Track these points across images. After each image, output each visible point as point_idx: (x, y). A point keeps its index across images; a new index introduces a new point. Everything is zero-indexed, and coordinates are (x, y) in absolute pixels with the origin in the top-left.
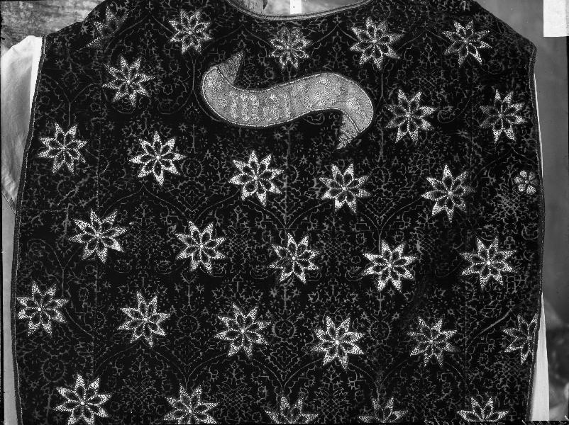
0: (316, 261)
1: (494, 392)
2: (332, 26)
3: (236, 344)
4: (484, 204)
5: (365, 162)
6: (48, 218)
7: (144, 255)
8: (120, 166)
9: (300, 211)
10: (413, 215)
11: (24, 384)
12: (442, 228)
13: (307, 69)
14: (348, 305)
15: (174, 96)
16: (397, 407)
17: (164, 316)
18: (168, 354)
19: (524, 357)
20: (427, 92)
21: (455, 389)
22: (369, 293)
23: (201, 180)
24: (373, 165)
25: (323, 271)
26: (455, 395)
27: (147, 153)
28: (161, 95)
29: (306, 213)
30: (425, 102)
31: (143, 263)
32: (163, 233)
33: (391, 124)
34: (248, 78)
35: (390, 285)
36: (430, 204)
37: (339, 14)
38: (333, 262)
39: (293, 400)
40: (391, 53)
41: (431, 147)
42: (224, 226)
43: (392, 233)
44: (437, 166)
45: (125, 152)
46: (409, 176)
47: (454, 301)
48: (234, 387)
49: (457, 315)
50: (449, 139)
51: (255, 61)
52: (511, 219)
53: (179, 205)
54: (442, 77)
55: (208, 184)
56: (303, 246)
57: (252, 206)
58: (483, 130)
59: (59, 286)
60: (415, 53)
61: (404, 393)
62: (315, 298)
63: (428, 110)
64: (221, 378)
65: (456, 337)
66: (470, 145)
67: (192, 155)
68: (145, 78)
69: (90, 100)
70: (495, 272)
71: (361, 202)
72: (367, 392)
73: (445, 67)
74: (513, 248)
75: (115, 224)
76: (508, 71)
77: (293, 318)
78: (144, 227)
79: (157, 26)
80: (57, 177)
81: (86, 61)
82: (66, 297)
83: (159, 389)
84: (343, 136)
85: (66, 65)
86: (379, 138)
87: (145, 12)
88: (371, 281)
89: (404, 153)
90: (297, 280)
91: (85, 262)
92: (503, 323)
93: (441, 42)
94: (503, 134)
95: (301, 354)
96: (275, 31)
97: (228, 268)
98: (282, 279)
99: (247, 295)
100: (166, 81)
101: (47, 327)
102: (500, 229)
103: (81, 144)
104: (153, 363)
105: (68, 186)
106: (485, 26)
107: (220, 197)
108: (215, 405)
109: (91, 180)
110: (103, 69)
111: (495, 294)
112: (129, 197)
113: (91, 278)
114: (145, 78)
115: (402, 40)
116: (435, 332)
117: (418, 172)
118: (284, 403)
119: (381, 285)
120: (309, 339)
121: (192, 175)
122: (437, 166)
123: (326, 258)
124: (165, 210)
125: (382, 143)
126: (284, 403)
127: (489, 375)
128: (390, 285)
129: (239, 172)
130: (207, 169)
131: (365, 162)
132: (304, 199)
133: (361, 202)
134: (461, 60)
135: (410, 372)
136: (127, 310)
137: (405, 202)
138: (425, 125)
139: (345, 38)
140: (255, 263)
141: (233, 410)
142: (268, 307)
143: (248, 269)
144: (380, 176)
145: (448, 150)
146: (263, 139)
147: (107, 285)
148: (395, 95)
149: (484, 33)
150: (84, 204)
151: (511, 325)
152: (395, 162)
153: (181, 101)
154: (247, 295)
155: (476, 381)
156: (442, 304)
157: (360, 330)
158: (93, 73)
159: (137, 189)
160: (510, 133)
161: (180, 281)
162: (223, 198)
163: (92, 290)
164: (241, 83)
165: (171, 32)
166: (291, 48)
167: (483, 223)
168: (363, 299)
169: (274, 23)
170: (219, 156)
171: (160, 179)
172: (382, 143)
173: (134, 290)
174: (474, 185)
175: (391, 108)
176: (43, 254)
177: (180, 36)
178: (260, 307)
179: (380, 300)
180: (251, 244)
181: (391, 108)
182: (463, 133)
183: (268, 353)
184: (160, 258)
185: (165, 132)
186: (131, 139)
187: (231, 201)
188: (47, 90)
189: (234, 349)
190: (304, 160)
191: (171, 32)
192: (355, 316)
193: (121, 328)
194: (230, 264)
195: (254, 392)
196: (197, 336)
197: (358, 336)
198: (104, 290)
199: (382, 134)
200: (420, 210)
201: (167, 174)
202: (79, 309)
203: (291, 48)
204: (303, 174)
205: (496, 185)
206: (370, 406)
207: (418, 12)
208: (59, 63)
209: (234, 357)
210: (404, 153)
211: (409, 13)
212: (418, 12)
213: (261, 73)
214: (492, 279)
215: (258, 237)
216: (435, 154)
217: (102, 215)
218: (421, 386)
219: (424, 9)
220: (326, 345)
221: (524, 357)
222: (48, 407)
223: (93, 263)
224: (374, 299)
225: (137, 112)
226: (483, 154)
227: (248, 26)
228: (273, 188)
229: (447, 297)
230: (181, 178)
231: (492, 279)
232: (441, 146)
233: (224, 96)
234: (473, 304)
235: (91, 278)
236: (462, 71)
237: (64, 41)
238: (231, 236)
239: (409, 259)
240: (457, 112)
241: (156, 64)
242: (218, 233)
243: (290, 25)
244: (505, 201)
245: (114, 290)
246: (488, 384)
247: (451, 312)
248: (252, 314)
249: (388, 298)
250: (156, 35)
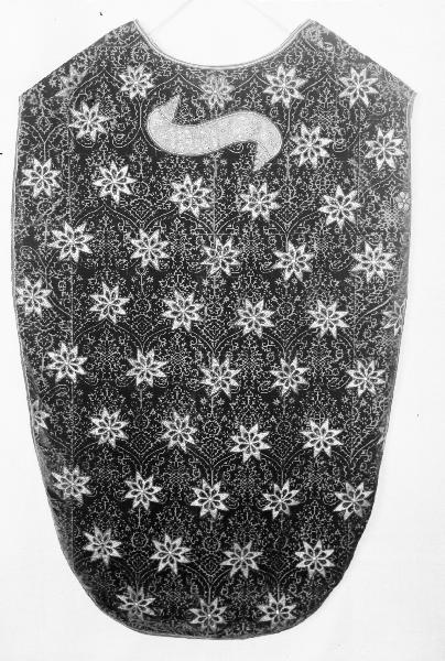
1: (376, 356)
3: (160, 555)
4: (370, 216)
5: (276, 181)
7: (107, 256)
8: (85, 189)
10: (312, 223)
12: (333, 233)
13: (229, 108)
14: (262, 291)
16: (300, 365)
17: (124, 301)
18: (128, 328)
19: (396, 330)
20: (325, 127)
21: (346, 355)
22: (278, 282)
23: (149, 198)
24: (281, 183)
25: (244, 266)
26: (346, 359)
28: (116, 132)
29: (232, 221)
30: (323, 135)
31: (107, 261)
32: (121, 238)
35: (294, 276)
37: (256, 65)
38: (251, 259)
39: (222, 360)
40: (297, 95)
41: (327, 171)
42: (167, 233)
43: (296, 236)
44: (331, 187)
45: (89, 178)
47: (345, 289)
50: (342, 162)
51: (189, 103)
52: (392, 230)
53: (131, 217)
55: (154, 201)
56: (228, 247)
57: (188, 217)
58: (368, 160)
62: (237, 286)
63: (325, 142)
64: (168, 345)
66: (357, 171)
67: (140, 179)
68: (102, 119)
69: (60, 137)
71: (273, 213)
72: (276, 353)
73: (339, 106)
74: (393, 251)
75: (85, 232)
76: (388, 114)
78: (106, 235)
79: (111, 79)
80: (37, 200)
81: (56, 107)
82: (49, 288)
83: (122, 353)
84: (256, 161)
85: (39, 111)
87: (100, 69)
88: (279, 273)
90: (224, 274)
91: (62, 262)
92: (383, 308)
93: (337, 87)
96: (204, 78)
97: (171, 264)
98: (212, 272)
99: (185, 284)
100: (119, 120)
101: (39, 310)
102: (384, 237)
103: (55, 173)
104: (116, 335)
105: (46, 207)
106: (376, 74)
107: (161, 212)
108: (165, 363)
110: (70, 113)
112: (93, 212)
115: (306, 85)
117: (317, 191)
119: (287, 276)
120: (233, 316)
121: (141, 195)
122: (331, 187)
123: (245, 256)
125: (288, 166)
126: (215, 363)
127: (372, 345)
128: (294, 276)
129: (177, 192)
130: (152, 190)
131: (276, 181)
132: (228, 211)
133: (273, 213)
135: (309, 339)
136: (95, 297)
137: (305, 213)
138: (324, 153)
139: (260, 83)
141: (177, 367)
143: (185, 265)
144: (287, 191)
145: (341, 175)
146: (197, 166)
148: (299, 129)
149: (374, 80)
150: (58, 218)
151: (390, 309)
154: (185, 284)
155: (362, 350)
158: (60, 116)
160: (391, 162)
161: (134, 274)
163: (68, 283)
164: (178, 120)
165: (121, 83)
166: (217, 92)
168: (273, 286)
170: (160, 180)
171: (116, 197)
172: (288, 166)
174: (361, 201)
175: (296, 139)
176: (31, 254)
177: (129, 86)
178: (196, 293)
180: (188, 246)
181: (296, 139)
182: (351, 161)
183: (202, 327)
185: (119, 162)
186: (94, 168)
188: (27, 134)
189: (176, 325)
190: (228, 181)
191: (121, 83)
194: (171, 261)
196: (150, 314)
198: (77, 283)
199: (288, 160)
200: (317, 220)
201: (122, 194)
202: (60, 297)
203: (217, 92)
204: (227, 192)
206: (279, 364)
207: (324, 58)
208: (34, 111)
211: (316, 58)
213: (194, 112)
214: (376, 275)
216: (330, 177)
217: (74, 226)
219: (330, 55)
220: (245, 320)
223: (68, 262)
224: (281, 286)
225: (97, 145)
226: (369, 177)
227: (184, 73)
229: (340, 287)
230: (133, 197)
232: (335, 171)
233: (164, 129)
235: (68, 274)
236: (352, 111)
238: (172, 240)
239: (308, 257)
240: (348, 145)
241: (111, 108)
242: (162, 238)
243: (217, 73)
244: (387, 214)
245: (85, 283)
246: (371, 351)
247: (344, 298)
249: (292, 285)
250: (110, 86)
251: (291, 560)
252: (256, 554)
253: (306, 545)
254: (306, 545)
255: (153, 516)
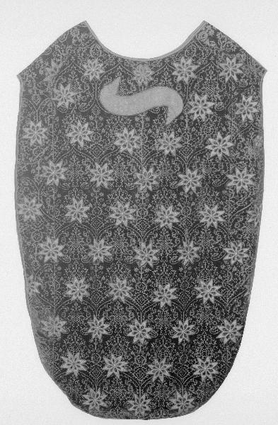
0: (157, 180)
2: (164, 63)
6: (29, 167)
8: (62, 139)
9: (148, 156)
10: (201, 156)
11: (24, 243)
14: (171, 200)
15: (87, 102)
19: (256, 224)
22: (181, 194)
24: (183, 132)
26: (223, 241)
27: (75, 131)
28: (81, 102)
30: (209, 100)
31: (75, 184)
32: (84, 169)
33: (192, 111)
34: (122, 90)
36: (209, 151)
39: (147, 244)
44: (214, 133)
46: (200, 137)
48: (119, 239)
49: (225, 204)
51: (126, 82)
54: (217, 88)
58: (237, 115)
59: (37, 198)
60: (204, 75)
61: (198, 239)
65: (224, 214)
67: (96, 131)
68: (72, 94)
70: (244, 184)
76: (249, 86)
77: (146, 207)
79: (77, 68)
80: (33, 147)
81: (44, 88)
86: (185, 118)
89: (198, 125)
92: (248, 209)
94: (247, 117)
95: (150, 223)
96: (135, 67)
97: (115, 184)
98: (141, 189)
100: (83, 94)
104: (82, 230)
105: (38, 151)
109: (50, 147)
111: (244, 195)
113: (52, 193)
114: (72, 94)
116: (213, 212)
117: (205, 136)
118: (143, 245)
122: (214, 133)
124: (84, 158)
125: (187, 121)
126: (143, 245)
127: (240, 232)
134: (227, 79)
140: (127, 182)
142: (135, 203)
144: (186, 137)
146: (131, 121)
147: (59, 196)
150: (46, 158)
152: (194, 129)
153: (91, 104)
156: (175, 277)
157: (178, 211)
158: (47, 93)
159: (70, 149)
161: (92, 191)
162: (111, 151)
166: (142, 76)
167: (238, 160)
168: (179, 197)
169: (135, 62)
172: (187, 121)
173: (71, 197)
175: (192, 103)
179: (186, 197)
181: (192, 103)
182: (227, 117)
184: (83, 181)
187: (115, 153)
192: (175, 204)
193: (67, 215)
195: (129, 241)
197: (176, 214)
198: (58, 199)
199: (187, 116)
203: (142, 76)
205: (245, 142)
208: (30, 91)
209: (119, 226)
210: (198, 125)
211: (205, 52)
212: (209, 51)
213: (129, 87)
214: (242, 188)
215: (129, 170)
218: (206, 237)
221: (256, 224)
222: (36, 253)
224: (183, 197)
226: (238, 126)
227: (123, 63)
228: (136, 146)
229: (220, 196)
231: (242, 188)
232: (217, 123)
234: (233, 199)
235: (52, 193)
236: (227, 84)
237: (32, 80)
243: (143, 64)
245: (62, 198)
247: (222, 203)
248: (127, 206)
250: (77, 72)
251: (190, 370)
252: (168, 366)
253: (200, 360)
254: (200, 360)
255: (104, 344)
